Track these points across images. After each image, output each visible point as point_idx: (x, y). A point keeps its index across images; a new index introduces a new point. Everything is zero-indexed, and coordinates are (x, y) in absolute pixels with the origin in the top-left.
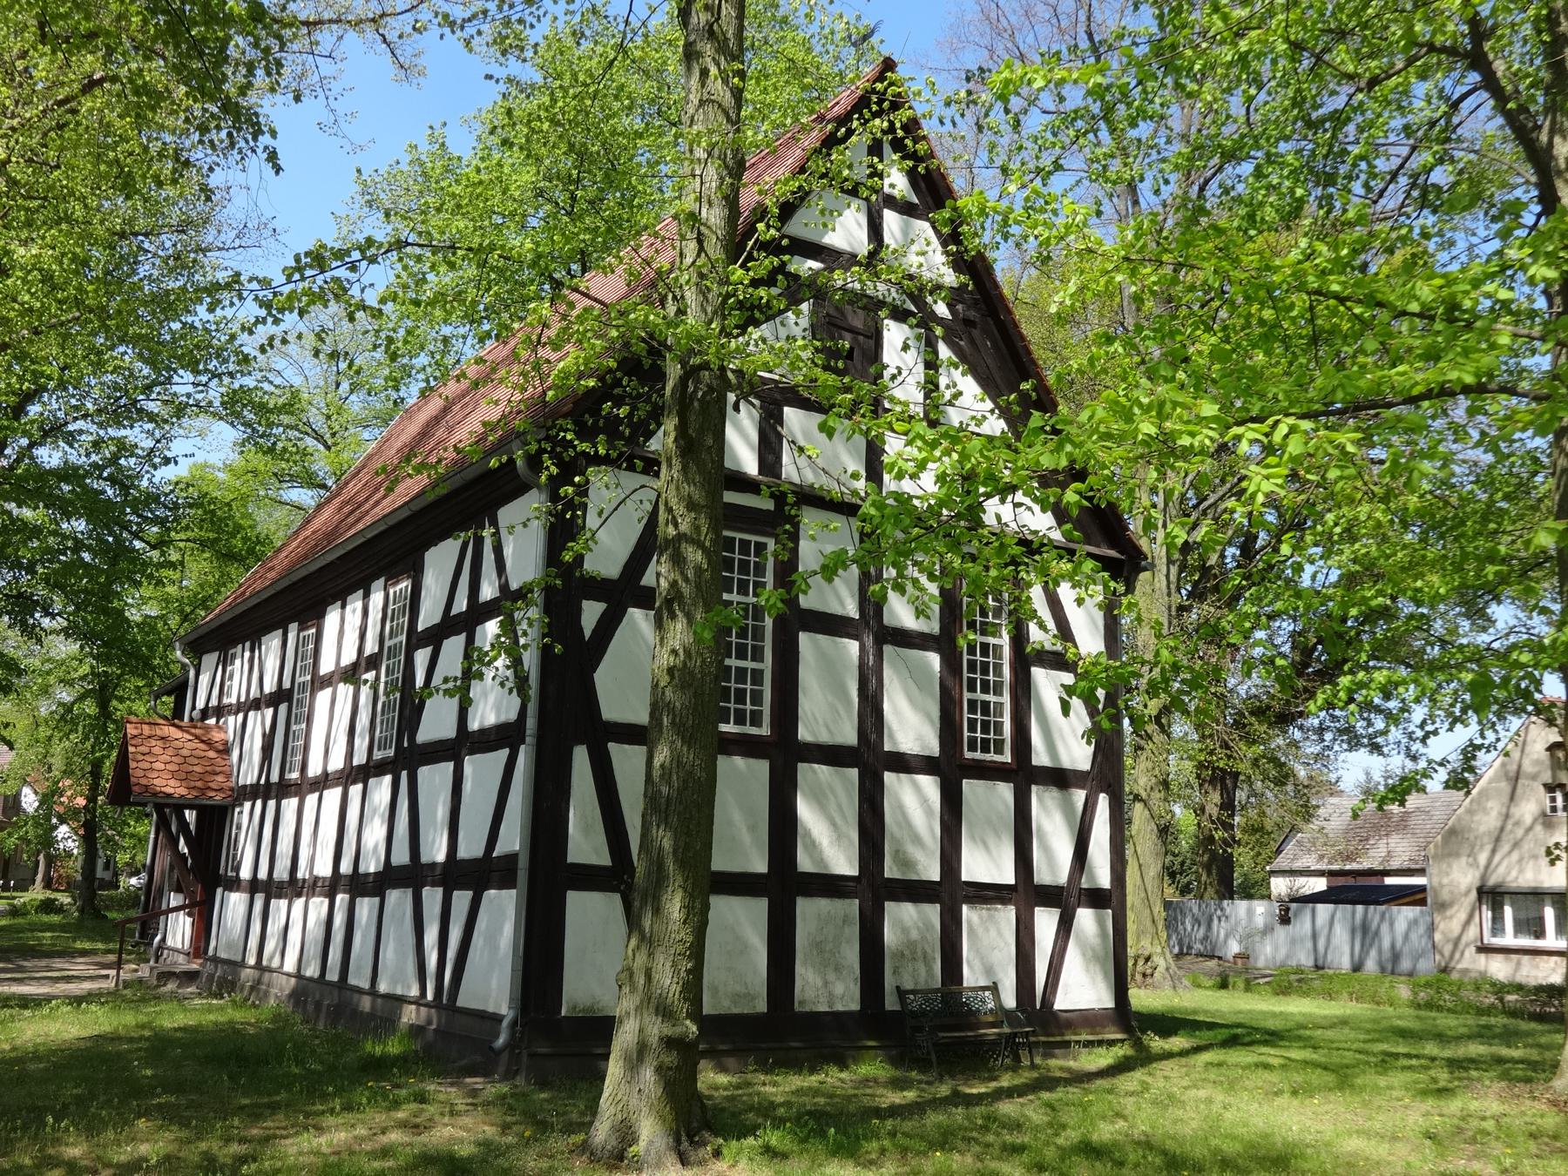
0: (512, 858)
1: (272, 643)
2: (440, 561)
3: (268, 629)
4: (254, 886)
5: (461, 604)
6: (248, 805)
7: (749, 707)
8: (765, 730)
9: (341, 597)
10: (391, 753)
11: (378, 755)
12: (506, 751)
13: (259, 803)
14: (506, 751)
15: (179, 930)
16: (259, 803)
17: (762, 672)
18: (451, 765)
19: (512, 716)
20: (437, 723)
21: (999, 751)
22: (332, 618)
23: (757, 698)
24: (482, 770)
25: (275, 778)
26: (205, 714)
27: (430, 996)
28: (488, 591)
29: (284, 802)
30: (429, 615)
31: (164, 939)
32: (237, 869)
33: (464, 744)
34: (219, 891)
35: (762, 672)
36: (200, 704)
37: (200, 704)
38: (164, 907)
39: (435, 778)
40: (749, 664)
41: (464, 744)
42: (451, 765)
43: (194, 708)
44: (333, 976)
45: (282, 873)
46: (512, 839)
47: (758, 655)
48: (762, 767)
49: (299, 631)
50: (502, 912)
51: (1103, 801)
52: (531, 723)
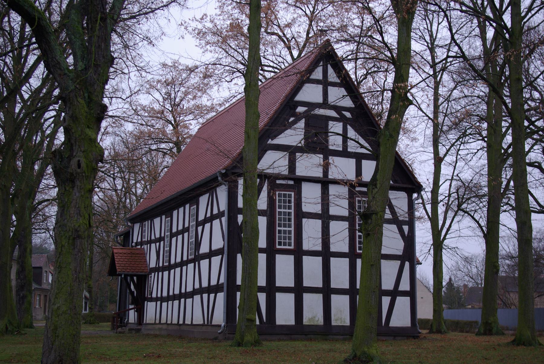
0: (223, 284)
1: (157, 221)
2: (204, 200)
3: (156, 216)
4: (156, 299)
5: (209, 215)
6: (153, 274)
7: (287, 241)
8: (292, 247)
9: (177, 207)
10: (193, 257)
11: (190, 257)
12: (221, 256)
13: (156, 273)
14: (221, 256)
15: (132, 316)
16: (156, 273)
17: (291, 231)
18: (208, 260)
19: (222, 246)
20: (204, 249)
21: (290, 245)
22: (175, 213)
23: (290, 238)
24: (216, 260)
25: (161, 265)
26: (137, 244)
27: (206, 323)
28: (215, 211)
29: (218, 294)
30: (201, 217)
31: (128, 321)
32: (151, 294)
33: (211, 254)
34: (146, 302)
35: (291, 231)
36: (135, 241)
37: (135, 241)
38: (127, 308)
39: (204, 263)
40: (287, 229)
41: (211, 254)
42: (208, 260)
43: (132, 242)
44: (181, 322)
45: (165, 294)
46: (222, 280)
47: (290, 226)
48: (291, 258)
49: (166, 218)
50: (221, 297)
51: (407, 264)
52: (226, 249)
